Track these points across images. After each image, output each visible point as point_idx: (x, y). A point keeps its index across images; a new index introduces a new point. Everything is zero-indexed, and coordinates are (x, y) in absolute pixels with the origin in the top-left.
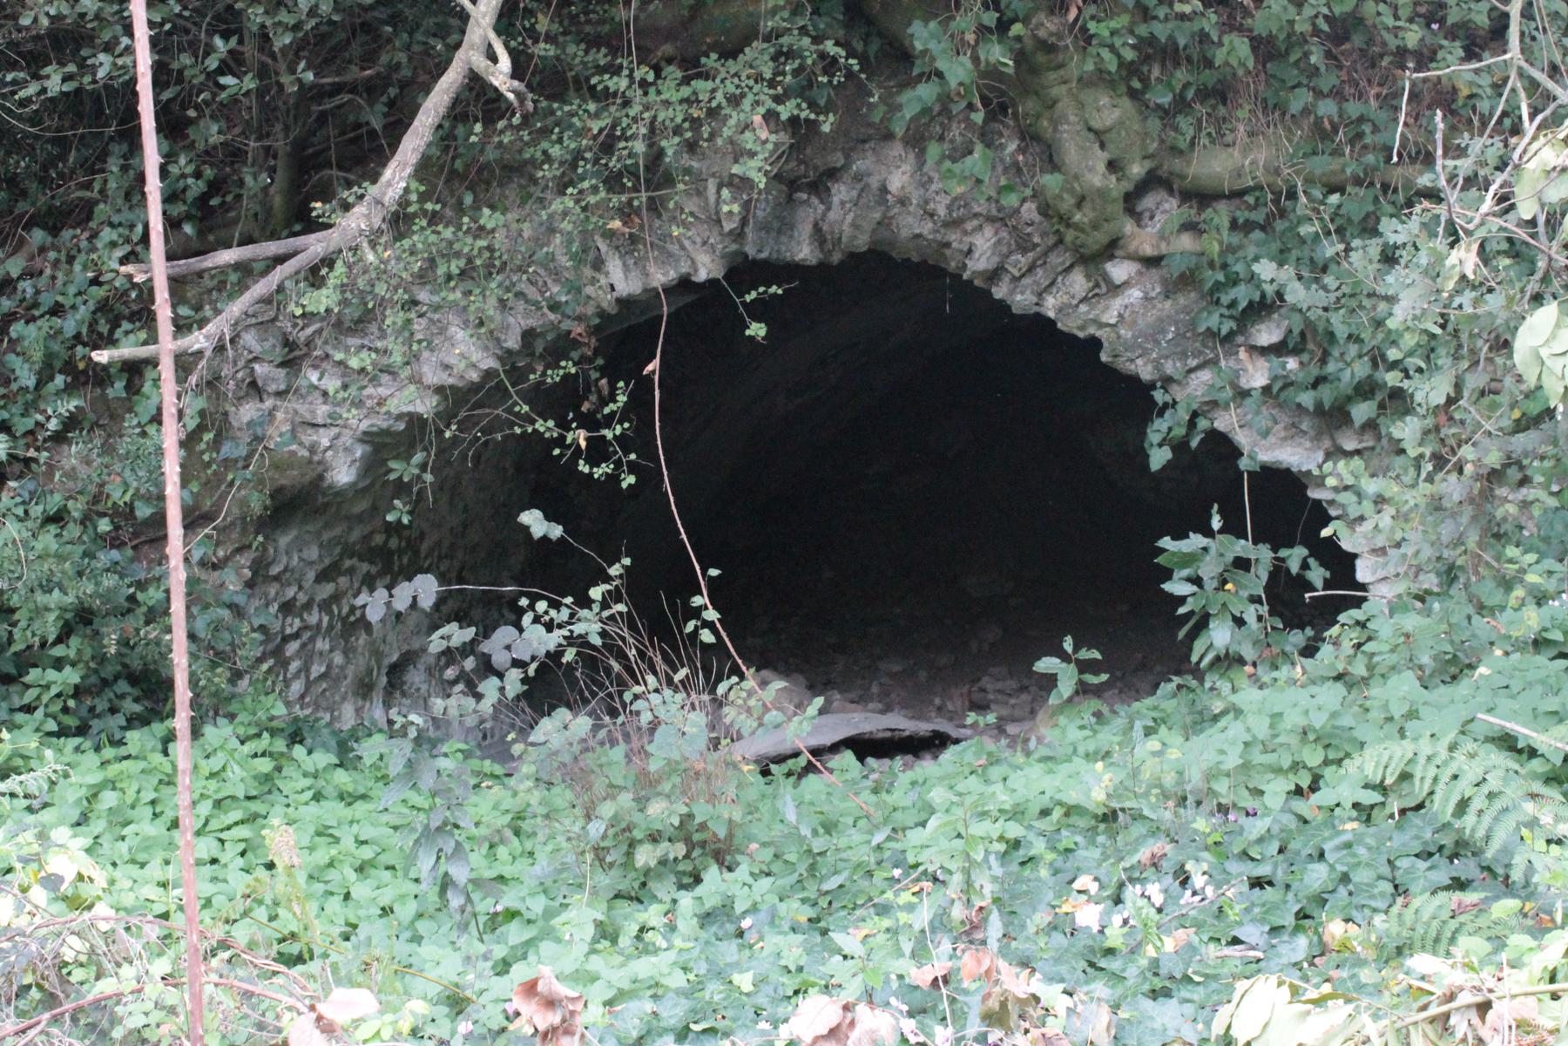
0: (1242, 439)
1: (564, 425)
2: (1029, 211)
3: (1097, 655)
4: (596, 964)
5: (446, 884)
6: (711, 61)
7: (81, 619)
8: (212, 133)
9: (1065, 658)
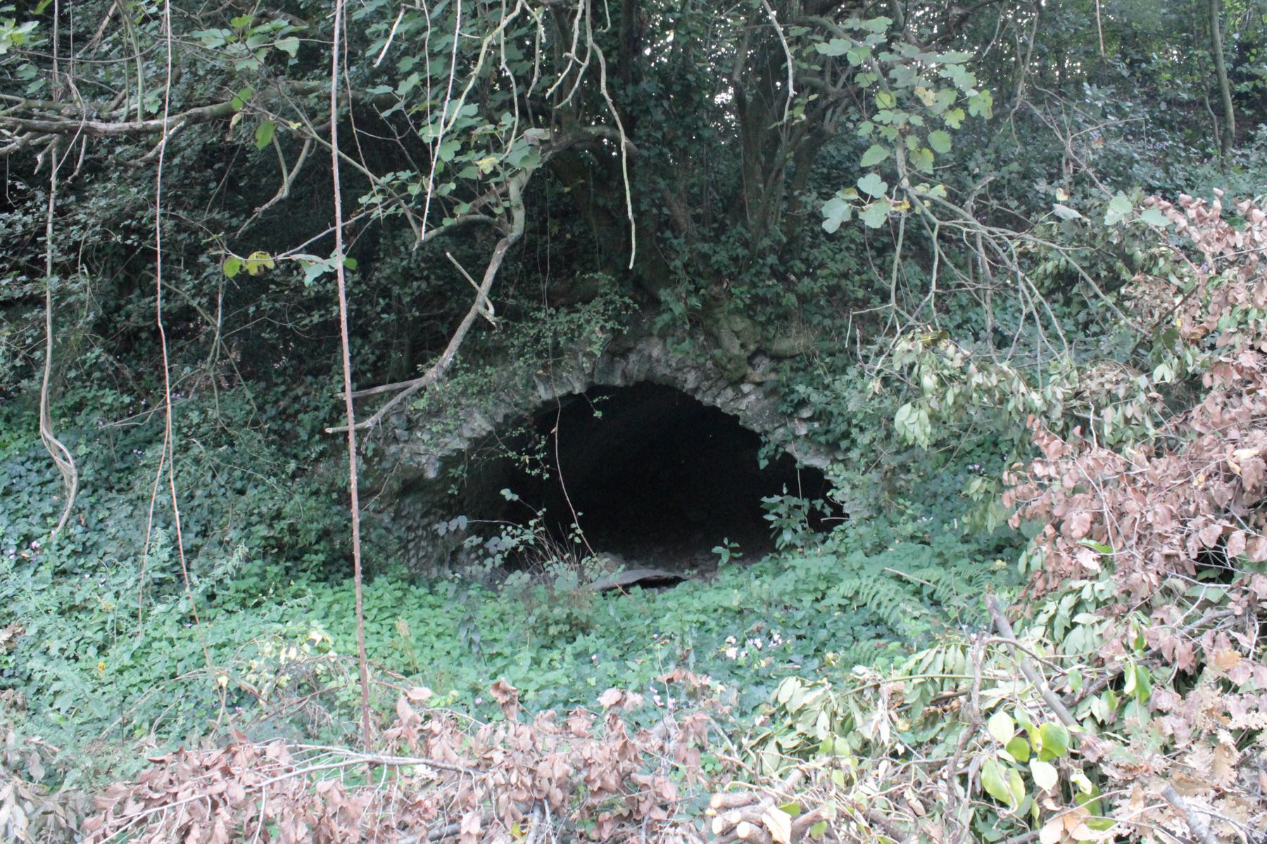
0: (797, 455)
1: (520, 454)
2: (709, 364)
4: (532, 675)
5: (471, 642)
6: (579, 305)
7: (325, 534)
8: (378, 336)
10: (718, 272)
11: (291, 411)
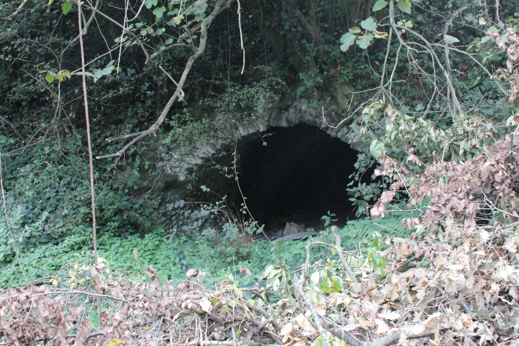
3: (334, 215)
7: (119, 212)
9: (328, 216)
10: (335, 61)
11: (103, 145)
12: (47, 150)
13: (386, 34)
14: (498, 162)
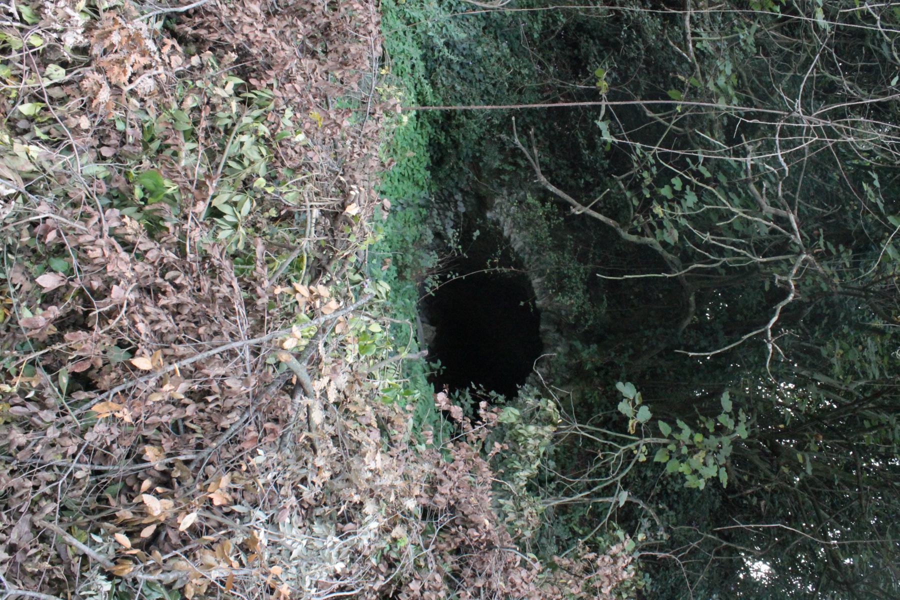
7: (456, 144)
10: (609, 384)
12: (525, 71)
13: (632, 432)
14: (488, 533)
